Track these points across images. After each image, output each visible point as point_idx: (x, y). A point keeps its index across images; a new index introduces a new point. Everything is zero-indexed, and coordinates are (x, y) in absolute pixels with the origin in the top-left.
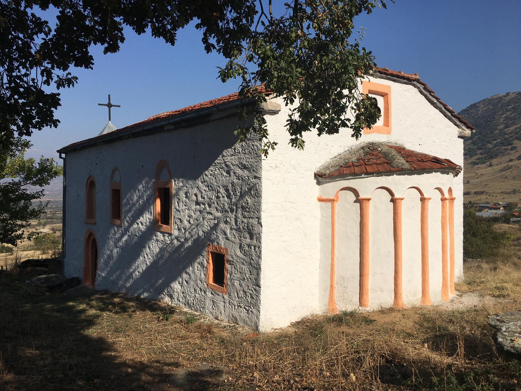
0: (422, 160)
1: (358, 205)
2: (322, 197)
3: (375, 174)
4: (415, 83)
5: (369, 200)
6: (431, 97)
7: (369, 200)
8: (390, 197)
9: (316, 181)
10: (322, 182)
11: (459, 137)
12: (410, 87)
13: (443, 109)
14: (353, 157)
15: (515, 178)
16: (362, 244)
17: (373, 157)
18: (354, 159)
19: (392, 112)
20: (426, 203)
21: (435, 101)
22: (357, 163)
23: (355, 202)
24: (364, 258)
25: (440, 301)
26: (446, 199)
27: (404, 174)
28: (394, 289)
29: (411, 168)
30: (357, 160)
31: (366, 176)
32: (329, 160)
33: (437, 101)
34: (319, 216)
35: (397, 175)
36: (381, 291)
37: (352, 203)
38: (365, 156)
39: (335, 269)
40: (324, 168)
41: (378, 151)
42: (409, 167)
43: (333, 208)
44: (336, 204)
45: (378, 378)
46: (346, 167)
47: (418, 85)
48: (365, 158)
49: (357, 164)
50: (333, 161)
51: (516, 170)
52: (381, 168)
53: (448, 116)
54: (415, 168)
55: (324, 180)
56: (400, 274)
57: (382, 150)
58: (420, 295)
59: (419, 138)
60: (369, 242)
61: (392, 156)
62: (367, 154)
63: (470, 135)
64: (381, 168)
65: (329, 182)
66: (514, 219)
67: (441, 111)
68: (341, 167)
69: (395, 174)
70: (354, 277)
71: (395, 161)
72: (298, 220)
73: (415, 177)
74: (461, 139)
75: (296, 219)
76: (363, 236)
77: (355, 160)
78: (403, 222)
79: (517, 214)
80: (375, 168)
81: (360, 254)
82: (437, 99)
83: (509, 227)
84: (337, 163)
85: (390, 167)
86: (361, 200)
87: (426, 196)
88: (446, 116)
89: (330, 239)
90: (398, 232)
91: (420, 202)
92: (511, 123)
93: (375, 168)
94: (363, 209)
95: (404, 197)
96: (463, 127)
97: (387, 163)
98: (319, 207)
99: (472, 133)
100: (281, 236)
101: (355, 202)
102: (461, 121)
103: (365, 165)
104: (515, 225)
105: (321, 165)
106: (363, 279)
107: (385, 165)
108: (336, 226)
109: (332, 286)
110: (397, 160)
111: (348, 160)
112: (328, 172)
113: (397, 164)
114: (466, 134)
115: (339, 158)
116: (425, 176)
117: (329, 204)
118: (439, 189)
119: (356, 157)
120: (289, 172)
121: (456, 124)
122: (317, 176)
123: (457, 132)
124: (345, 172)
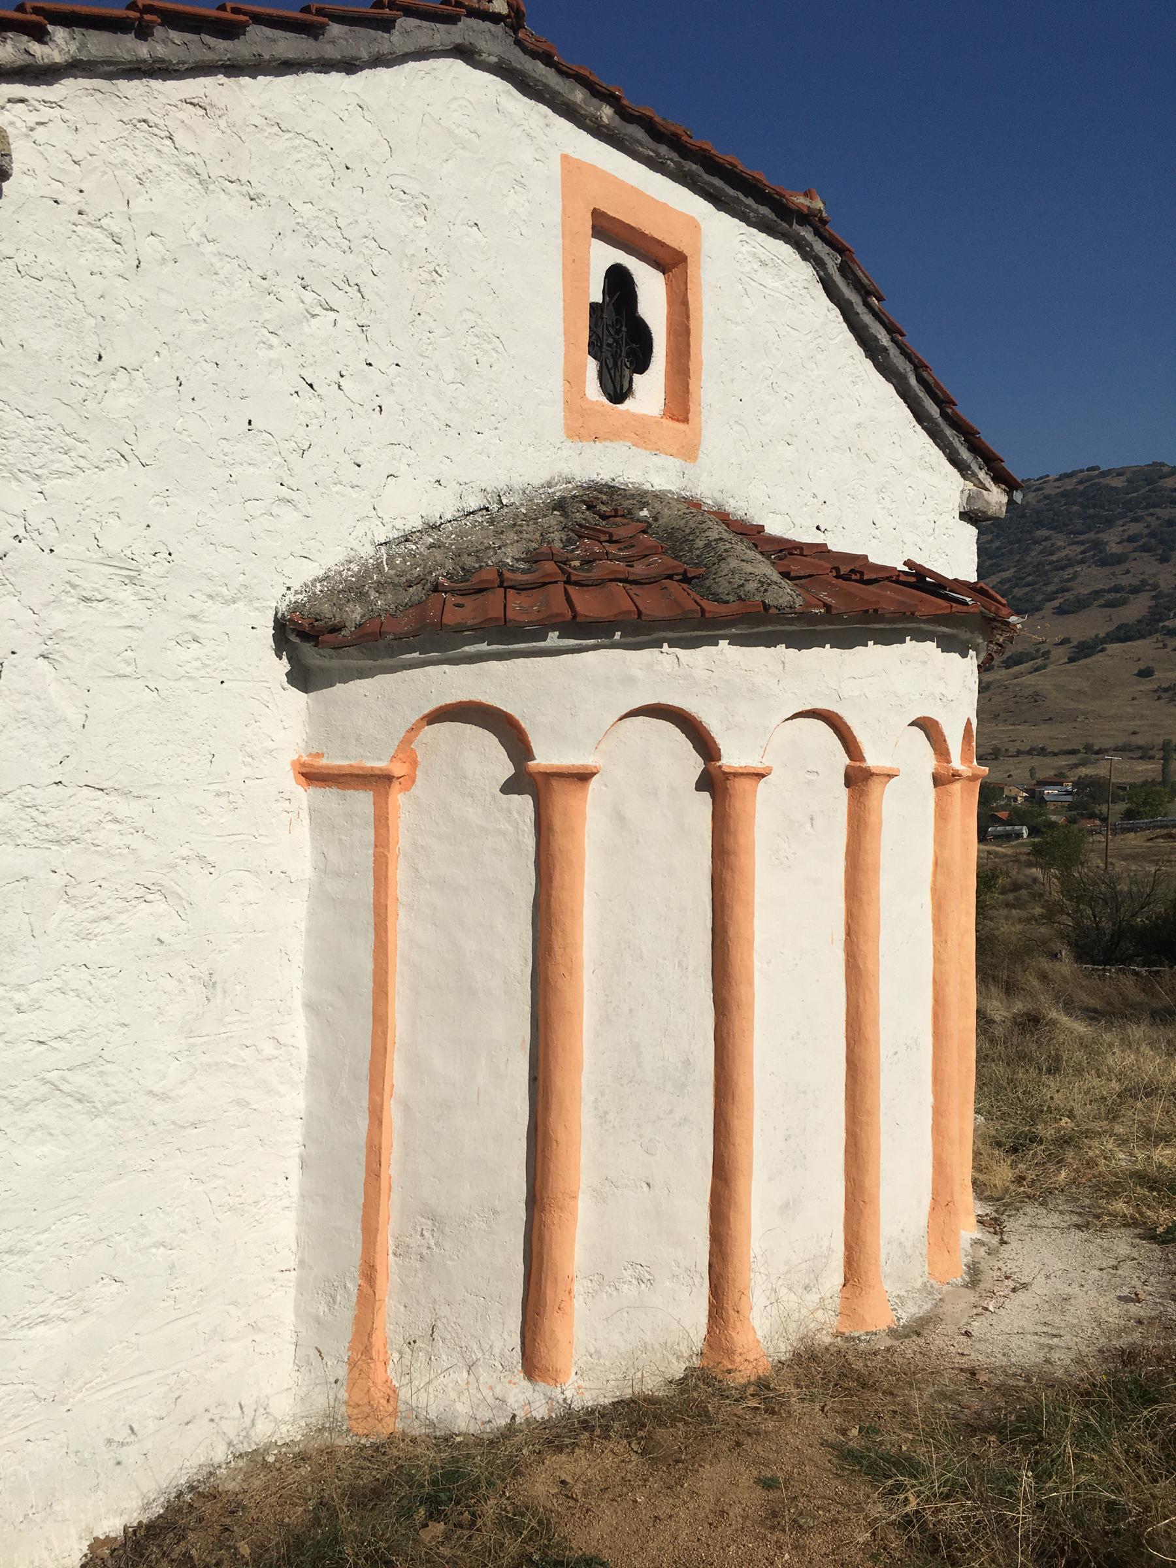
0: (853, 571)
1: (523, 804)
2: (324, 762)
3: (618, 635)
4: (806, 233)
5: (583, 777)
6: (867, 318)
7: (583, 777)
8: (695, 765)
9: (288, 668)
10: (322, 670)
11: (965, 516)
12: (784, 250)
13: (913, 381)
14: (505, 545)
15: (996, 716)
16: (541, 1024)
17: (613, 549)
18: (510, 554)
19: (705, 355)
20: (872, 800)
21: (884, 339)
22: (524, 572)
23: (509, 788)
24: (554, 1106)
25: (925, 1285)
26: (956, 776)
27: (769, 641)
28: (710, 1265)
29: (807, 604)
30: (525, 561)
31: (572, 642)
32: (368, 551)
33: (893, 340)
34: (303, 866)
35: (735, 641)
36: (640, 1280)
37: (494, 797)
38: (569, 541)
39: (393, 1168)
40: (331, 594)
41: (638, 520)
42: (799, 602)
43: (382, 822)
44: (399, 799)
45: (651, 153)
46: (464, 593)
47: (820, 248)
48: (573, 550)
49: (520, 577)
50: (390, 559)
51: (1000, 694)
52: (651, 603)
53: (929, 418)
54: (828, 607)
55: (335, 663)
56: (740, 1184)
57: (656, 519)
58: (834, 1278)
59: (815, 496)
60: (580, 1014)
61: (707, 546)
62: (580, 532)
63: (1004, 509)
64: (651, 603)
65: (362, 674)
66: (999, 828)
67: (905, 394)
68: (436, 588)
69: (724, 637)
70: (495, 1212)
71: (725, 568)
72: (158, 896)
73: (824, 657)
74: (969, 526)
75: (141, 891)
76: (547, 980)
77: (518, 560)
78: (758, 898)
79: (1003, 815)
80: (621, 600)
81: (533, 1079)
82: (891, 330)
83: (989, 853)
84: (414, 566)
85: (698, 598)
86: (539, 779)
87: (873, 759)
88: (920, 416)
89: (366, 1001)
90: (736, 954)
91: (843, 793)
92: (991, 565)
93: (621, 600)
94: (550, 828)
95: (767, 762)
96: (982, 475)
97: (686, 579)
98: (305, 815)
99: (1011, 502)
100: (19, 1010)
101: (509, 788)
102: (976, 448)
103: (568, 582)
104: (1000, 846)
105: (320, 573)
106: (543, 1223)
107: (673, 586)
108: (402, 923)
109: (369, 1272)
110: (734, 563)
111: (479, 559)
112: (355, 613)
113: (737, 581)
114: (988, 503)
115: (431, 546)
116: (872, 654)
117: (362, 800)
118: (928, 727)
119: (523, 545)
120: (86, 600)
121: (955, 461)
122: (293, 638)
123: (958, 493)
124: (452, 617)
